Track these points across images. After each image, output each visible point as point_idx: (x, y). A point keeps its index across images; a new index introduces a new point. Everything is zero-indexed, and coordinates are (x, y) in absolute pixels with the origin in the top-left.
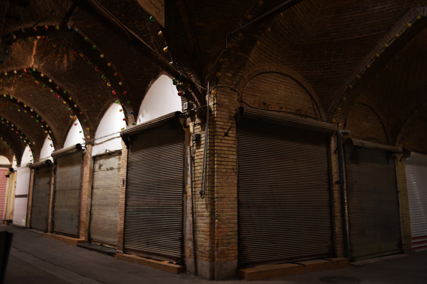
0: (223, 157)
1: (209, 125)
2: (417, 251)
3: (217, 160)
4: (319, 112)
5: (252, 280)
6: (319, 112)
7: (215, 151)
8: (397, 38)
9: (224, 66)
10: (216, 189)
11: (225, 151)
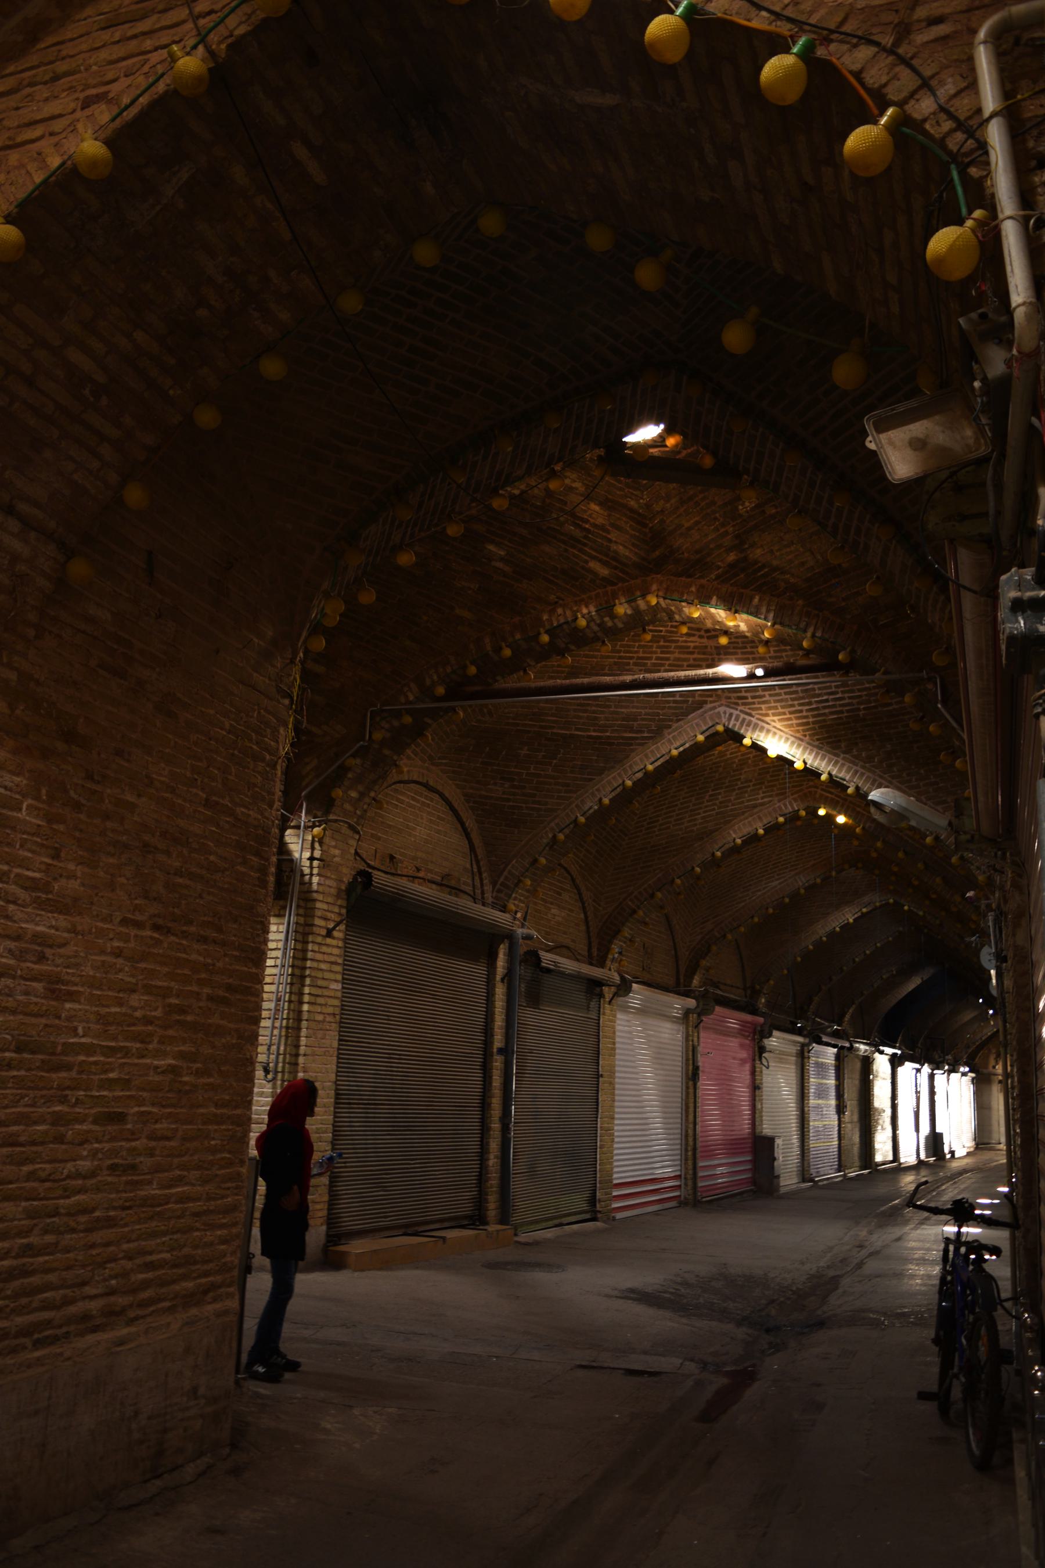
0: (320, 987)
1: (298, 906)
2: (619, 1215)
3: (309, 994)
4: (481, 880)
5: (362, 1270)
6: (481, 880)
7: (308, 972)
8: (672, 758)
9: (350, 775)
10: (301, 1060)
11: (325, 973)
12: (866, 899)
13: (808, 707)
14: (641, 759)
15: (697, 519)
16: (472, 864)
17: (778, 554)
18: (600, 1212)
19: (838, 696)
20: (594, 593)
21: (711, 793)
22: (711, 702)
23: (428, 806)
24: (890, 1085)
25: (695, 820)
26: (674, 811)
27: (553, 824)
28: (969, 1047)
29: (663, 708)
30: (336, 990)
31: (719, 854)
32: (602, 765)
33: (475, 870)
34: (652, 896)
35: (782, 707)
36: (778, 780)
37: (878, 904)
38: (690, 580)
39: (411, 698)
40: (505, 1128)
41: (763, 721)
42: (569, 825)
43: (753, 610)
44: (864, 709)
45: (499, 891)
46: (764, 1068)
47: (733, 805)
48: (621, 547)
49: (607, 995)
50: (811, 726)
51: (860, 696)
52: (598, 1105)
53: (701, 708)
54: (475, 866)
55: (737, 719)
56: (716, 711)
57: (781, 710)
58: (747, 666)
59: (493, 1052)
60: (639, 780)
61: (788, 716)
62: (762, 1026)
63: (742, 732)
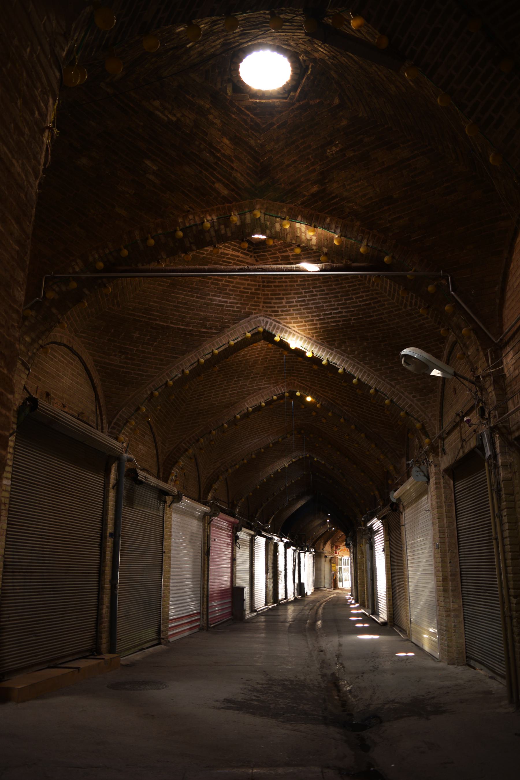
4: (102, 420)
6: (102, 420)
12: (294, 454)
13: (317, 318)
14: (210, 347)
15: (295, 158)
16: (96, 408)
17: (348, 187)
18: (163, 639)
19: (338, 311)
20: (215, 207)
21: (236, 379)
22: (255, 314)
23: (72, 364)
24: (284, 558)
25: (226, 395)
26: (214, 389)
27: (151, 385)
28: (313, 539)
29: (226, 315)
30: (7, 485)
31: (238, 416)
32: (185, 348)
33: (98, 413)
34: (198, 441)
35: (301, 318)
36: (274, 374)
37: (301, 457)
38: (282, 204)
39: (77, 269)
40: (113, 587)
41: (287, 327)
42: (162, 386)
43: (326, 226)
44: (354, 319)
45: (113, 428)
46: (237, 548)
47: (248, 388)
48: (239, 175)
49: (168, 503)
50: (318, 330)
51: (353, 311)
52: (162, 571)
53: (249, 316)
54: (98, 410)
55: (271, 325)
56: (258, 319)
57: (299, 320)
58: (318, 264)
59: (106, 535)
60: (208, 359)
61: (304, 324)
62: (237, 524)
63: (274, 332)
